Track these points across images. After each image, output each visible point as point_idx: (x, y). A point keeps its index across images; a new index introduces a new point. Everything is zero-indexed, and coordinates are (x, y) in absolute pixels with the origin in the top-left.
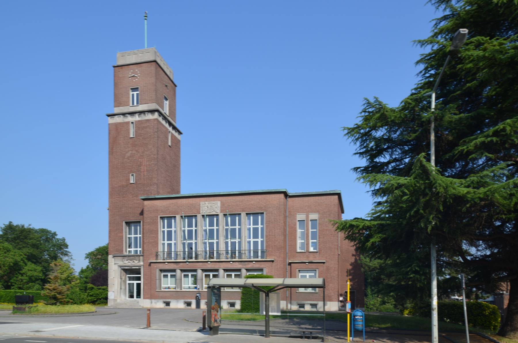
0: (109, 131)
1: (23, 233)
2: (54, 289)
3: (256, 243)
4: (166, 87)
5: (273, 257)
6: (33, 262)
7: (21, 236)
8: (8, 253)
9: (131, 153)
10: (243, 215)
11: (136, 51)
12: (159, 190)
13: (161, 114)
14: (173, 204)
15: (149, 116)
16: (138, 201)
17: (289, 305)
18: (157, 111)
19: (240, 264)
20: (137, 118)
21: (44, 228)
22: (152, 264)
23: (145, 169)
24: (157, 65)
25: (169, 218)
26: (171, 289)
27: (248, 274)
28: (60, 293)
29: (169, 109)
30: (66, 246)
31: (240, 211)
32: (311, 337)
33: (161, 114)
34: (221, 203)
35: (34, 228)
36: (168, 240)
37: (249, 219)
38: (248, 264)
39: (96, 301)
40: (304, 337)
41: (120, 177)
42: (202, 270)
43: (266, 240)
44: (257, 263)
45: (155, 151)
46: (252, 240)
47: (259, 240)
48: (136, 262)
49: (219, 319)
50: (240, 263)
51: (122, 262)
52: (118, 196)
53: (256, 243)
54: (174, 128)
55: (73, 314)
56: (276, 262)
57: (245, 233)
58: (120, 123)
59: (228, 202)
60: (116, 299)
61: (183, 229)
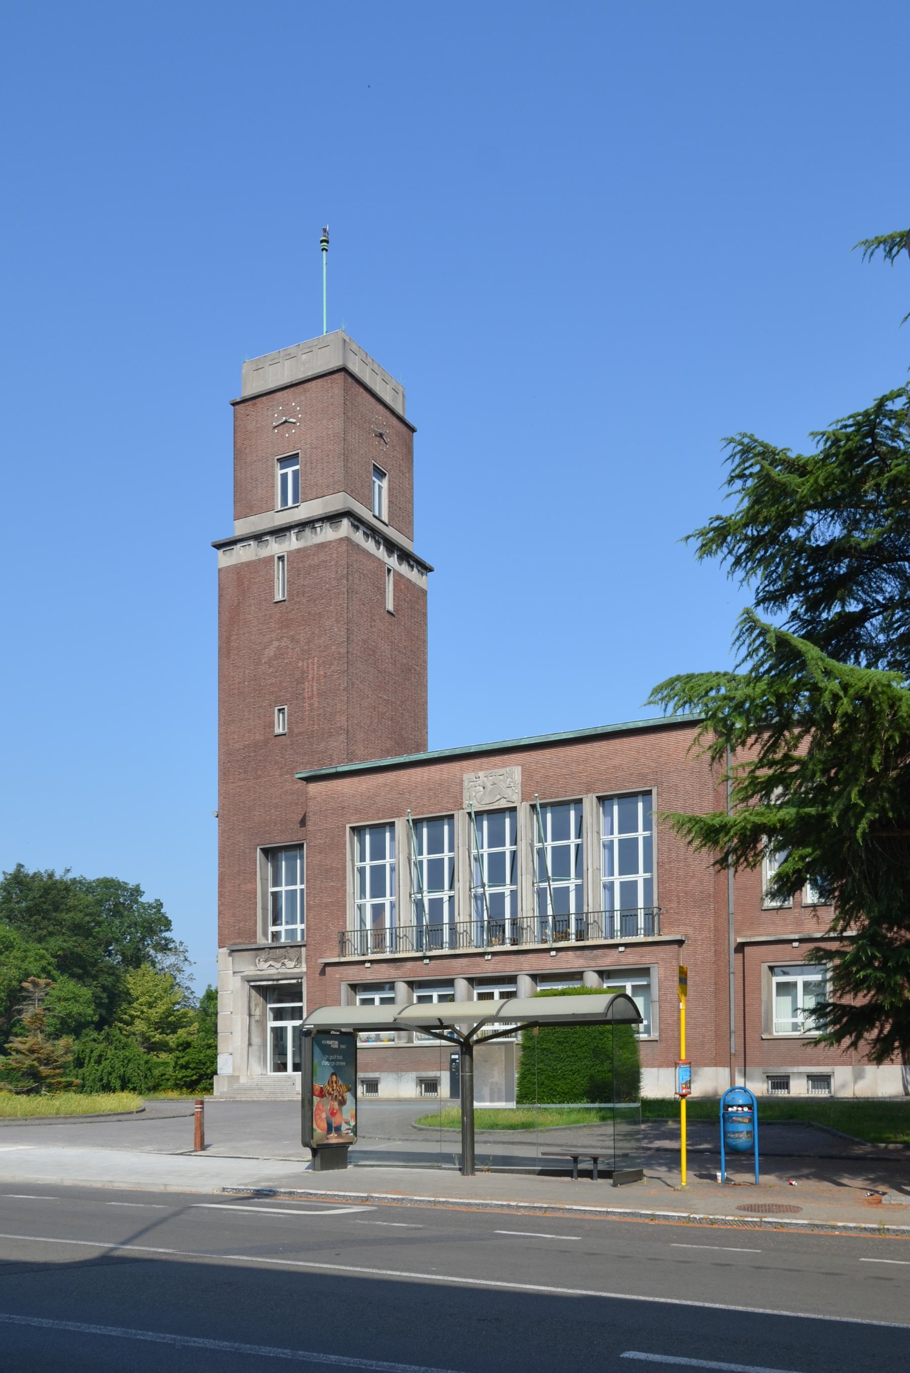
0: (220, 589)
1: (48, 894)
2: (32, 1051)
3: (629, 889)
4: (378, 439)
5: (683, 929)
6: (72, 975)
7: (45, 903)
8: (7, 953)
9: (279, 648)
10: (590, 803)
11: (292, 349)
12: (354, 747)
13: (358, 522)
14: (385, 785)
15: (327, 534)
16: (297, 786)
17: (739, 1082)
18: (348, 514)
19: (578, 957)
20: (293, 542)
21: (109, 875)
22: (328, 969)
23: (315, 688)
24: (350, 380)
25: (378, 829)
26: (382, 1041)
27: (539, 989)
28: (47, 1062)
29: (390, 502)
30: (168, 924)
31: (580, 793)
32: (595, 1173)
33: (358, 522)
34: (523, 771)
35: (84, 879)
36: (373, 896)
37: (480, 829)
38: (605, 956)
39: (197, 1082)
40: (575, 1174)
41: (249, 719)
42: (471, 981)
43: (658, 877)
44: (629, 950)
45: (342, 633)
46: (618, 879)
47: (640, 877)
48: (291, 964)
49: (347, 1123)
50: (579, 953)
51: (252, 968)
52: (242, 776)
53: (629, 889)
54: (406, 556)
55: (70, 1117)
56: (689, 945)
57: (594, 858)
58: (248, 564)
59: (544, 767)
60: (237, 1074)
61: (537, 845)
